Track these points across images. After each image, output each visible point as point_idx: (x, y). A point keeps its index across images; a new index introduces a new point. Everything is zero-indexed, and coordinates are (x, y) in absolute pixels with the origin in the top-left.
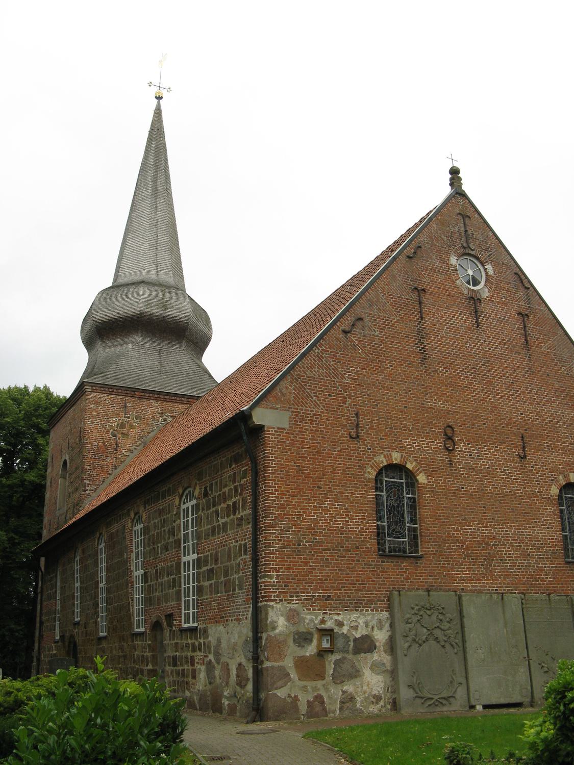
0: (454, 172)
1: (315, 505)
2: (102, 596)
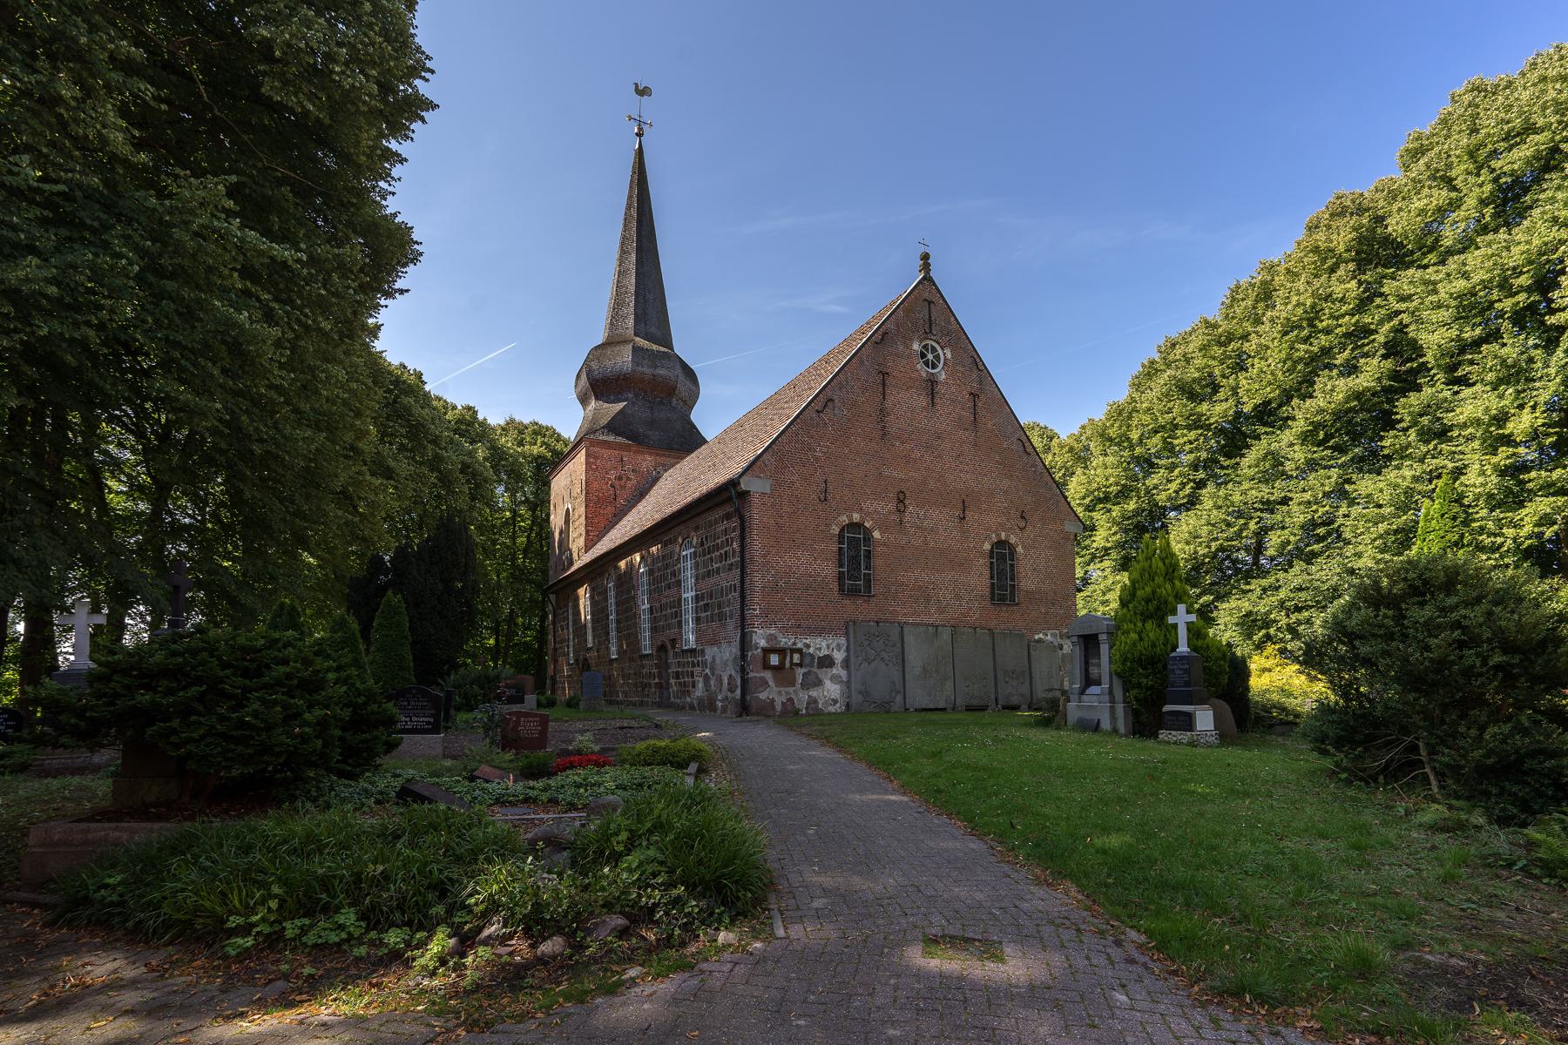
0: (925, 257)
1: (795, 559)
2: (613, 626)
